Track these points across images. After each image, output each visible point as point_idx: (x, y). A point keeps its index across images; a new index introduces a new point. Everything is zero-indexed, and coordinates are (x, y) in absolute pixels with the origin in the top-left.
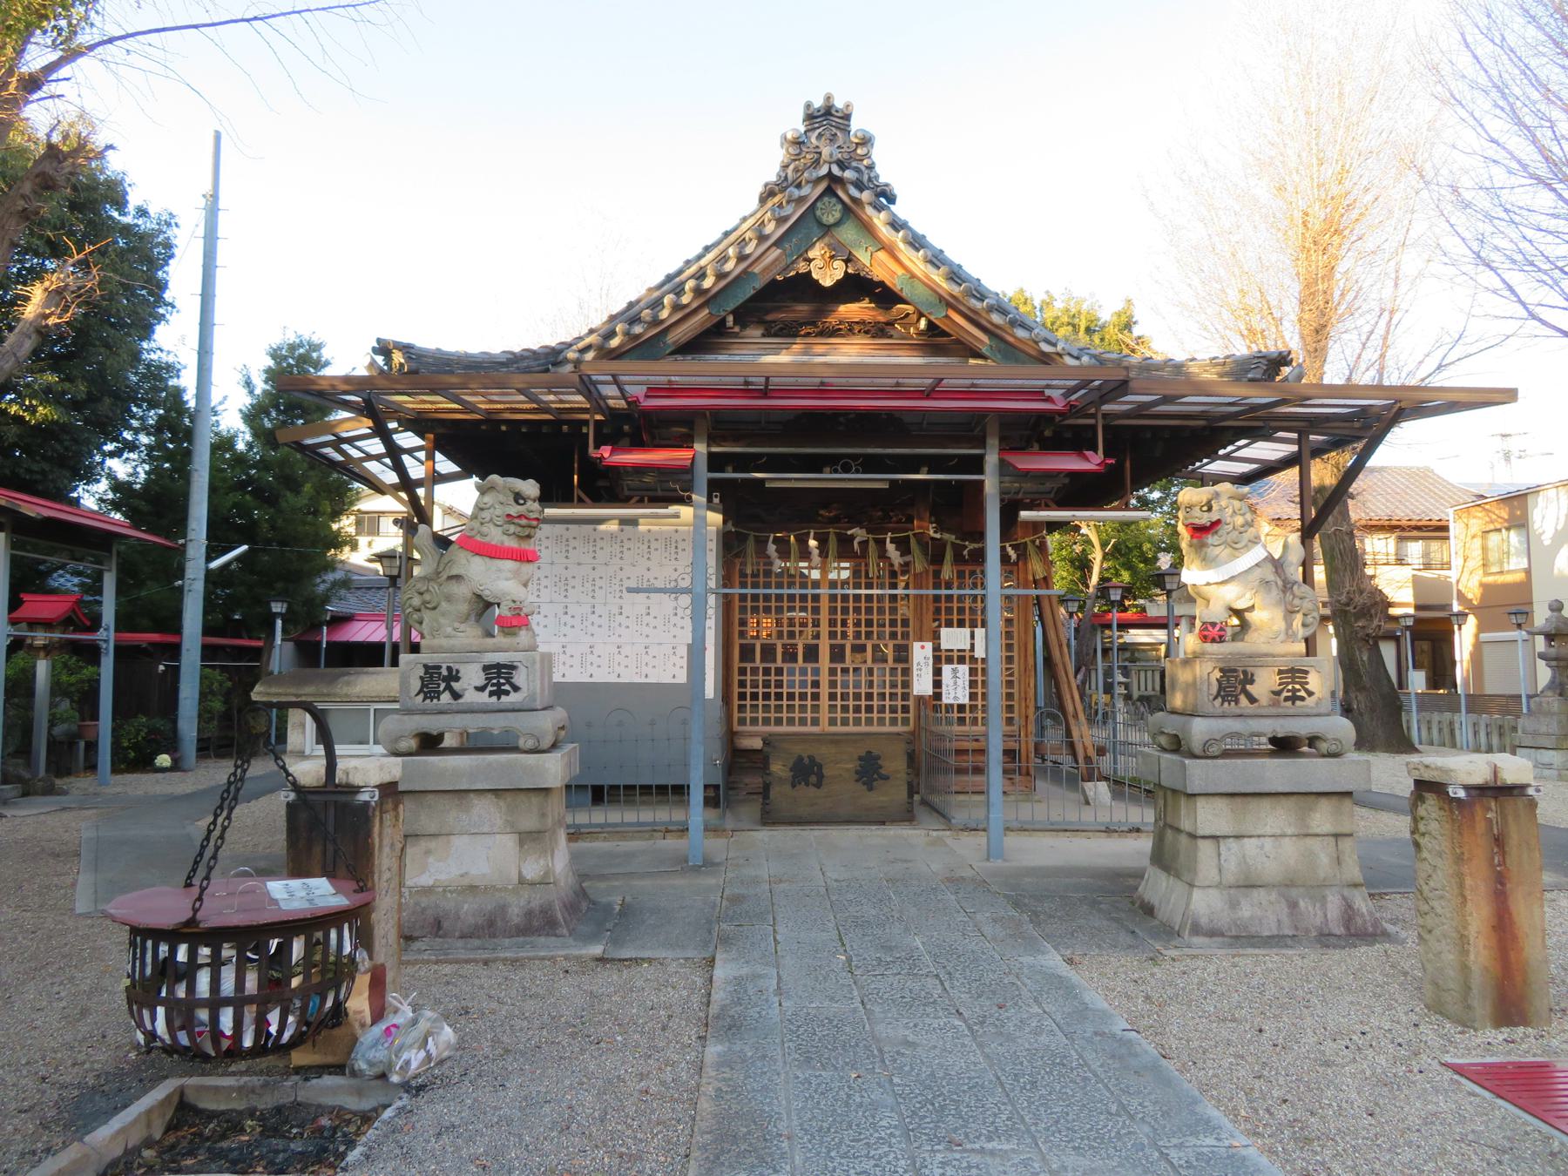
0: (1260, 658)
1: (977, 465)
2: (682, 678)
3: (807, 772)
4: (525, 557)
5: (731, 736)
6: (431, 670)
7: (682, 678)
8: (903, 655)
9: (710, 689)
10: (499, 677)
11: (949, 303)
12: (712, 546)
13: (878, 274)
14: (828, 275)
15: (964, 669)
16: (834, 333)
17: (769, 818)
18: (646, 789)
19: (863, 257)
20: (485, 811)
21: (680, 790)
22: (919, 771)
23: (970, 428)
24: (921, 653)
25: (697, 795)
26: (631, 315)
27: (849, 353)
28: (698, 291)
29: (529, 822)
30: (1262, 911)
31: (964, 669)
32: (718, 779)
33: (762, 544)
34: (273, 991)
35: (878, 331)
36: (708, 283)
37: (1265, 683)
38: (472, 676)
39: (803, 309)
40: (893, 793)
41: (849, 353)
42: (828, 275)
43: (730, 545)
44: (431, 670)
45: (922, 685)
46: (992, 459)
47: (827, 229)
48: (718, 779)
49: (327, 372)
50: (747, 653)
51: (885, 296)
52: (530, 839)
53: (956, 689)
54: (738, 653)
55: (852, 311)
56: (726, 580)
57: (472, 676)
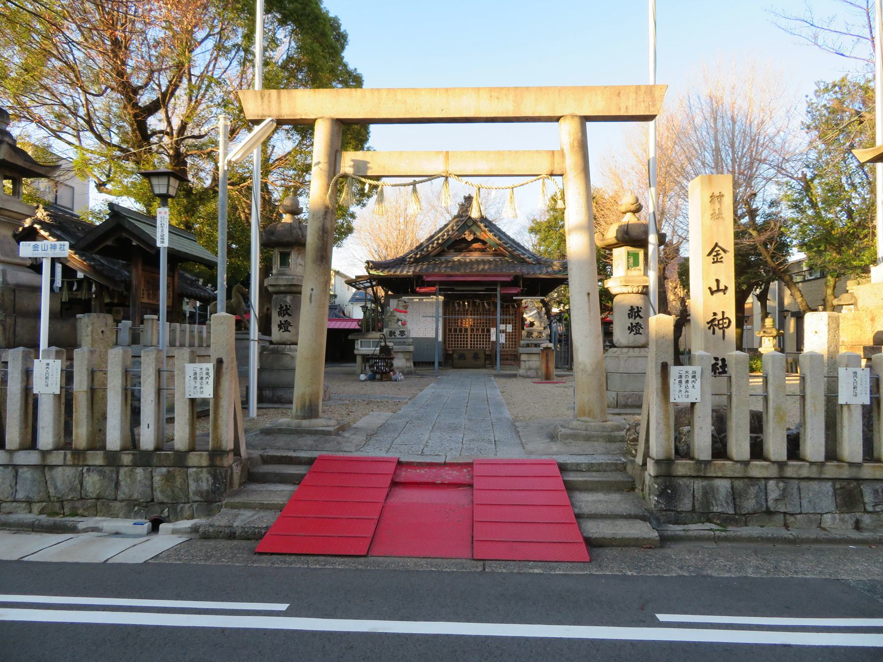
0: (535, 330)
1: (496, 290)
2: (434, 336)
3: (462, 357)
4: (406, 312)
5: (445, 350)
6: (391, 332)
7: (434, 336)
8: (489, 331)
9: (440, 339)
10: (402, 333)
11: (499, 245)
12: (441, 305)
13: (482, 238)
14: (470, 238)
15: (504, 335)
16: (471, 251)
17: (454, 367)
18: (426, 363)
19: (478, 234)
20: (401, 355)
21: (433, 363)
22: (486, 359)
23: (495, 283)
24: (493, 330)
25: (436, 364)
26: (420, 247)
27: (475, 256)
28: (438, 243)
29: (408, 357)
30: (532, 373)
31: (504, 335)
32: (442, 360)
33: (454, 303)
34: (387, 366)
35: (482, 250)
36: (440, 241)
37: (535, 334)
38: (397, 333)
39: (464, 245)
40: (481, 362)
41: (475, 256)
42: (470, 238)
43: (446, 304)
44: (391, 332)
45: (493, 338)
46: (499, 289)
47: (469, 227)
48: (442, 360)
49: (334, 249)
50: (450, 330)
51: (484, 242)
52: (407, 360)
53: (502, 339)
54: (448, 329)
55: (476, 245)
56: (445, 314)
57: (397, 333)
